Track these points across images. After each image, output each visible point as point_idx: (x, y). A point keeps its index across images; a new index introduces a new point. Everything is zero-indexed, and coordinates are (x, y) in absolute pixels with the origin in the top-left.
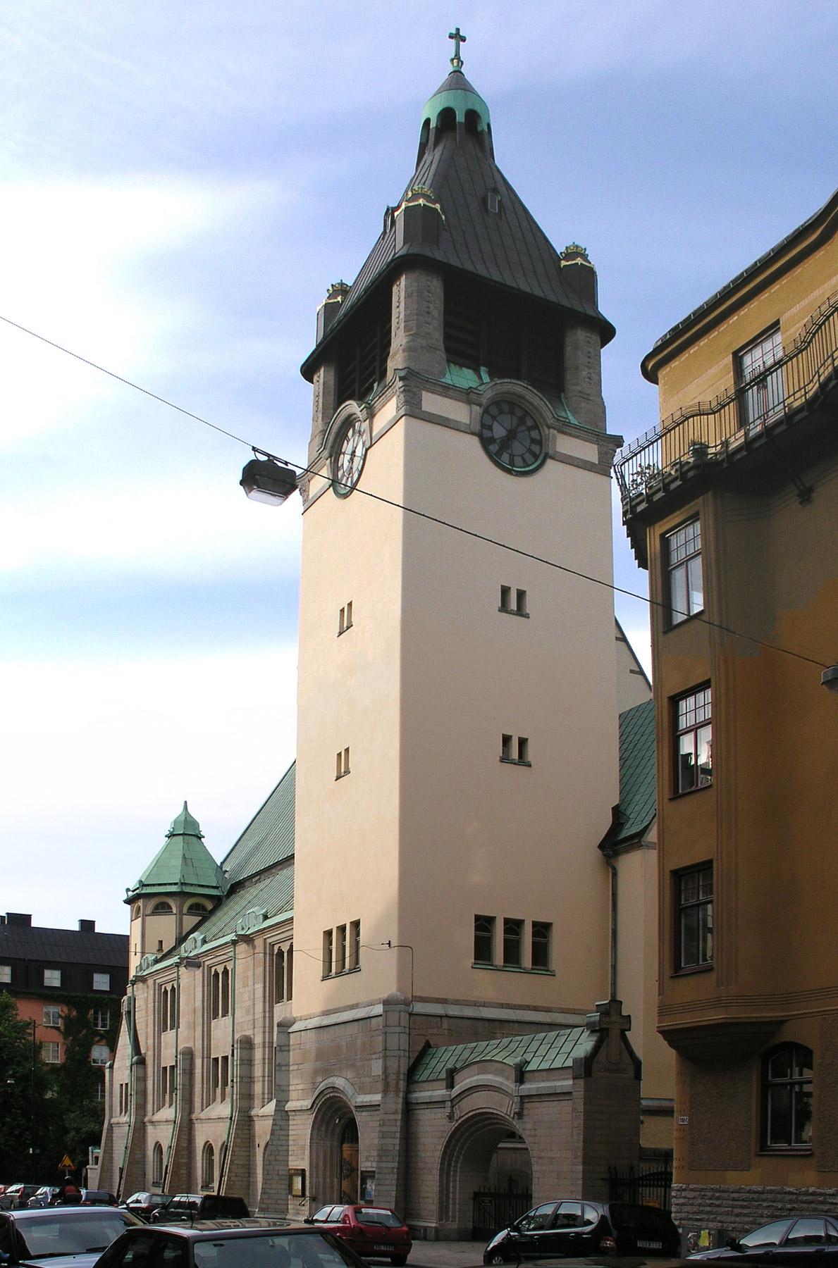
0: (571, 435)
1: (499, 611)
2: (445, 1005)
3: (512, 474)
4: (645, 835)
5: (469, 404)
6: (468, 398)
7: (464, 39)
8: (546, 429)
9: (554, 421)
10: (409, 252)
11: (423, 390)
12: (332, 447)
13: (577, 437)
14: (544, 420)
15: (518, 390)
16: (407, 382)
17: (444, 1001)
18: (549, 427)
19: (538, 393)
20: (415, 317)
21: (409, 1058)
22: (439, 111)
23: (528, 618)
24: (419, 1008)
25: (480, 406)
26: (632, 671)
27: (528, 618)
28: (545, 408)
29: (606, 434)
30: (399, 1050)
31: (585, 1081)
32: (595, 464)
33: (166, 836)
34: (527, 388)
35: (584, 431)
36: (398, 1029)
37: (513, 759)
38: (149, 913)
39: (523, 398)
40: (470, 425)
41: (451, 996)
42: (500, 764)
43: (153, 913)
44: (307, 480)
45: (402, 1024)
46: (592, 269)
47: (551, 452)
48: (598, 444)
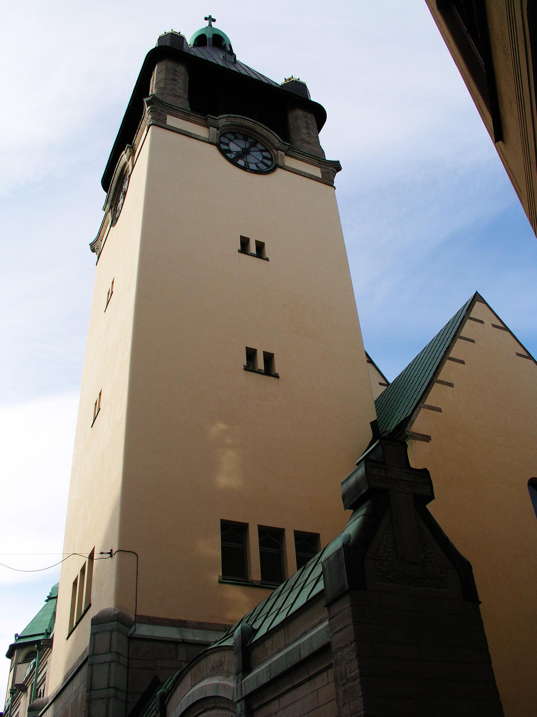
0: (296, 158)
1: (239, 252)
2: (183, 629)
3: (247, 171)
4: (409, 425)
5: (208, 128)
6: (207, 123)
7: (214, 20)
8: (275, 152)
9: (281, 145)
10: (159, 45)
11: (168, 114)
12: (112, 200)
13: (302, 160)
14: (273, 145)
15: (250, 124)
16: (154, 106)
17: (181, 624)
18: (277, 149)
19: (265, 127)
20: (164, 80)
21: (127, 702)
22: (196, 37)
23: (268, 260)
24: (143, 630)
25: (218, 128)
26: (380, 384)
27: (268, 260)
28: (273, 137)
29: (325, 160)
30: (109, 687)
31: (207, 138)
32: (320, 178)
33: (46, 601)
34: (256, 123)
35: (307, 156)
36: (108, 657)
37: (259, 369)
38: (20, 661)
39: (253, 130)
40: (209, 139)
41: (192, 618)
42: (244, 372)
43: (24, 661)
44: (100, 240)
45: (114, 649)
46: (305, 84)
47: (280, 163)
48: (320, 167)
